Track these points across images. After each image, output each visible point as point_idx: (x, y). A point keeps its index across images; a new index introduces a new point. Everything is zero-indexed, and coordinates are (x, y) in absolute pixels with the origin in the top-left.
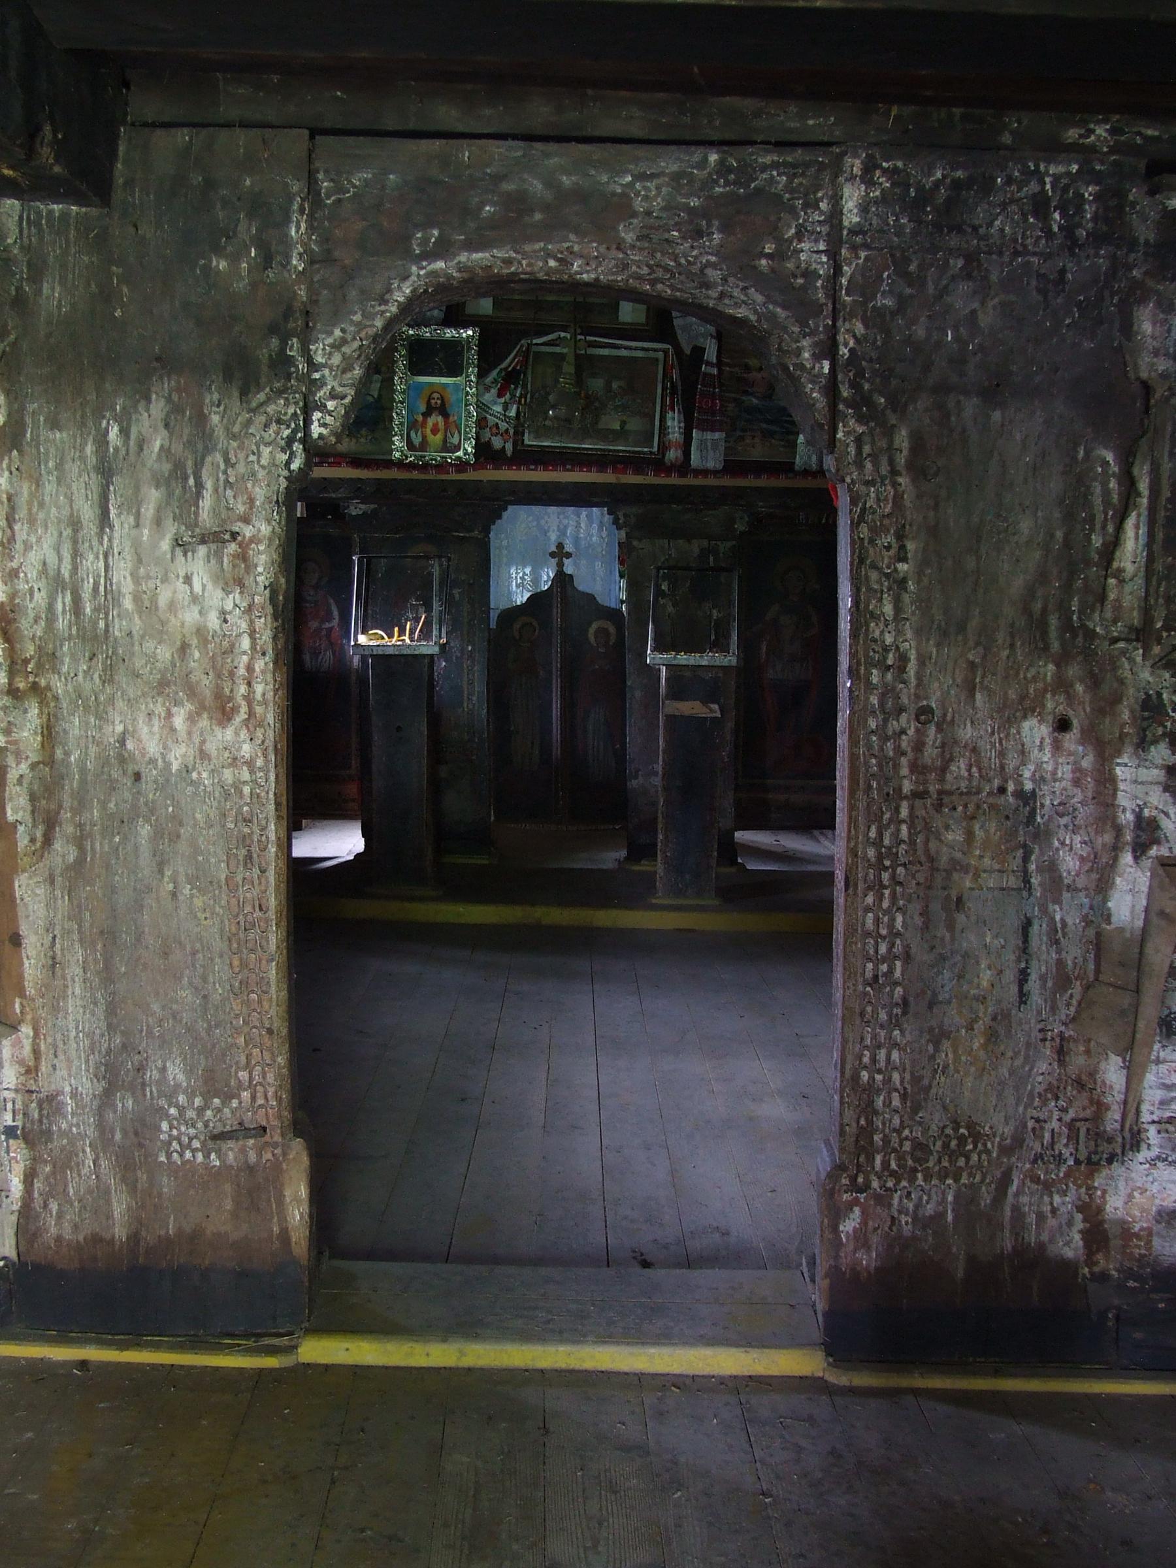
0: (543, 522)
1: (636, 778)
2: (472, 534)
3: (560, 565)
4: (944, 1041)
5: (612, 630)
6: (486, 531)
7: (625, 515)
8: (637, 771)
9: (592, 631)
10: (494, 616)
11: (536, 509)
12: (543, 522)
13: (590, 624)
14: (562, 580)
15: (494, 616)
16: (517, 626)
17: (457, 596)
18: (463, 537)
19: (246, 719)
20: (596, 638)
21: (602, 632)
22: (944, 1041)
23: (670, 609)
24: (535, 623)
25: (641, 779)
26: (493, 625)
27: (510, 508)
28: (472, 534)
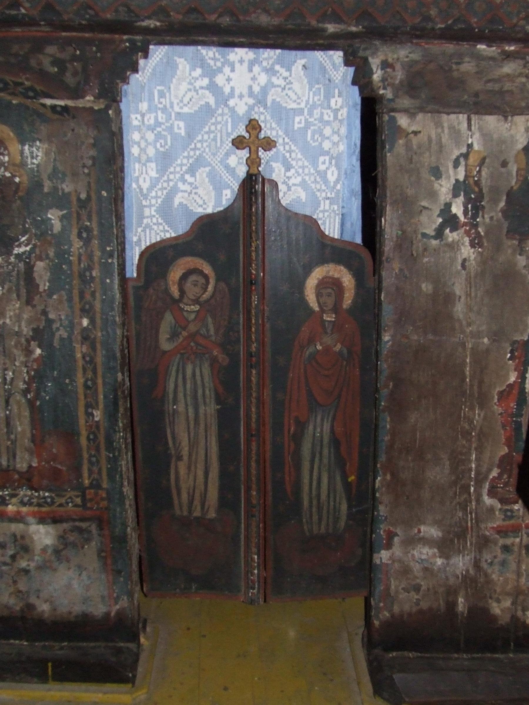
0: (220, 80)
1: (389, 546)
2: (80, 103)
3: (253, 162)
4: (257, 66)
5: (348, 280)
6: (112, 96)
7: (385, 65)
8: (391, 535)
9: (312, 282)
10: (133, 256)
11: (209, 53)
12: (220, 80)
13: (308, 270)
14: (253, 188)
15: (133, 256)
16: (175, 274)
17: (57, 226)
18: (66, 109)
19: (232, 98)
20: (319, 295)
21: (331, 285)
22: (257, 66)
23: (467, 251)
24: (207, 269)
25: (397, 550)
26: (132, 272)
27: (159, 53)
28: (80, 103)
